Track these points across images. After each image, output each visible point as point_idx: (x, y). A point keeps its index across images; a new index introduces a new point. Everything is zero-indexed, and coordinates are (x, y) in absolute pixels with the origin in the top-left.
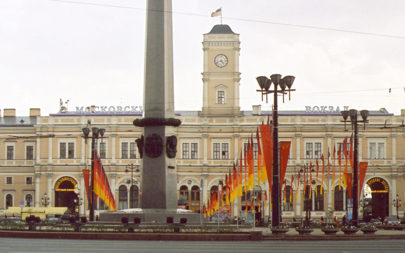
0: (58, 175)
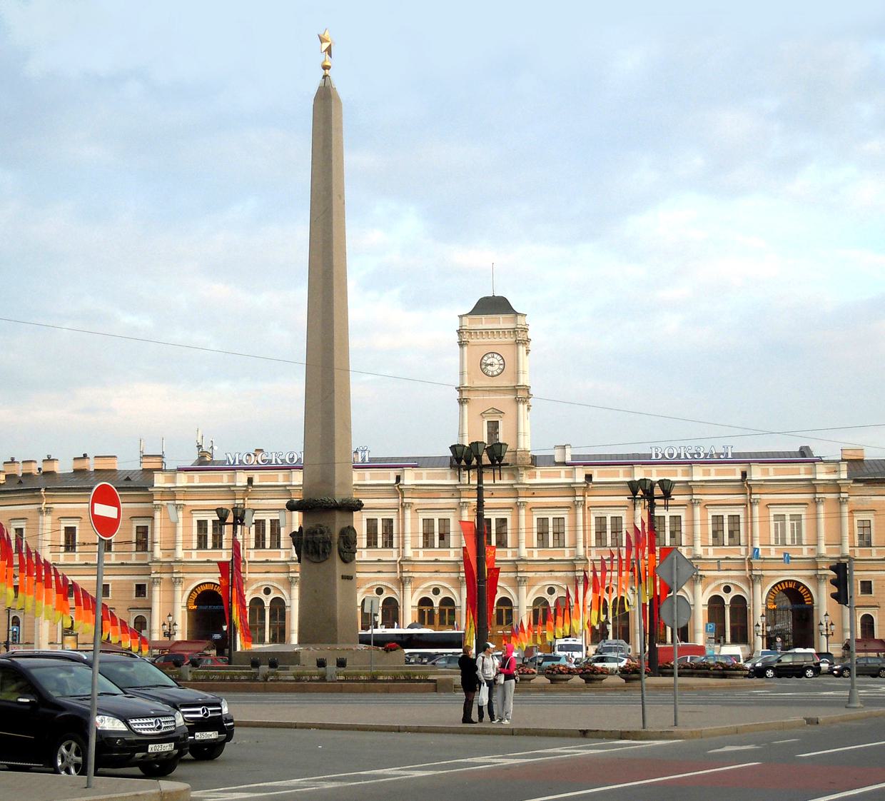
0: (193, 580)
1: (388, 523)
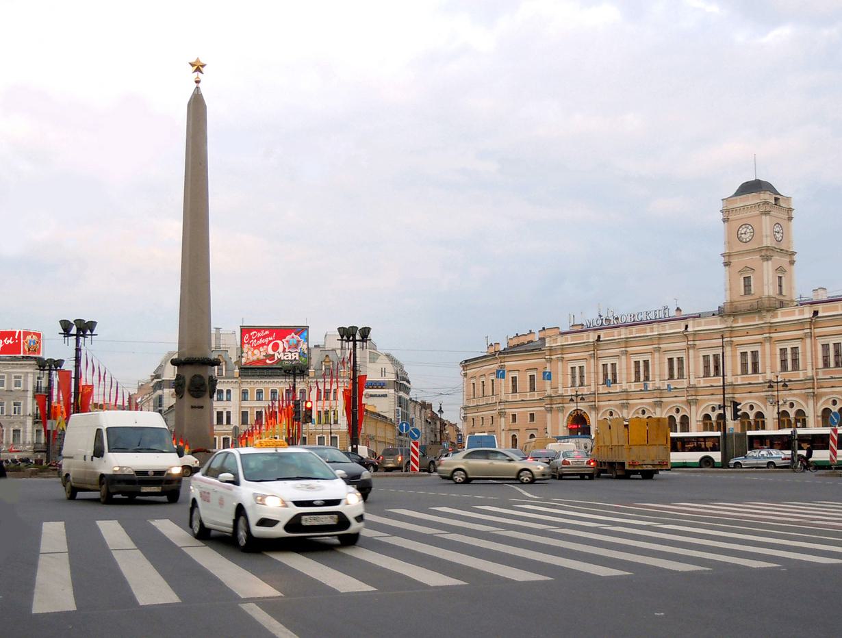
1: (680, 360)
